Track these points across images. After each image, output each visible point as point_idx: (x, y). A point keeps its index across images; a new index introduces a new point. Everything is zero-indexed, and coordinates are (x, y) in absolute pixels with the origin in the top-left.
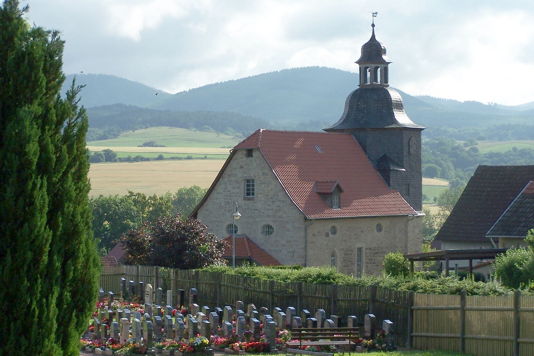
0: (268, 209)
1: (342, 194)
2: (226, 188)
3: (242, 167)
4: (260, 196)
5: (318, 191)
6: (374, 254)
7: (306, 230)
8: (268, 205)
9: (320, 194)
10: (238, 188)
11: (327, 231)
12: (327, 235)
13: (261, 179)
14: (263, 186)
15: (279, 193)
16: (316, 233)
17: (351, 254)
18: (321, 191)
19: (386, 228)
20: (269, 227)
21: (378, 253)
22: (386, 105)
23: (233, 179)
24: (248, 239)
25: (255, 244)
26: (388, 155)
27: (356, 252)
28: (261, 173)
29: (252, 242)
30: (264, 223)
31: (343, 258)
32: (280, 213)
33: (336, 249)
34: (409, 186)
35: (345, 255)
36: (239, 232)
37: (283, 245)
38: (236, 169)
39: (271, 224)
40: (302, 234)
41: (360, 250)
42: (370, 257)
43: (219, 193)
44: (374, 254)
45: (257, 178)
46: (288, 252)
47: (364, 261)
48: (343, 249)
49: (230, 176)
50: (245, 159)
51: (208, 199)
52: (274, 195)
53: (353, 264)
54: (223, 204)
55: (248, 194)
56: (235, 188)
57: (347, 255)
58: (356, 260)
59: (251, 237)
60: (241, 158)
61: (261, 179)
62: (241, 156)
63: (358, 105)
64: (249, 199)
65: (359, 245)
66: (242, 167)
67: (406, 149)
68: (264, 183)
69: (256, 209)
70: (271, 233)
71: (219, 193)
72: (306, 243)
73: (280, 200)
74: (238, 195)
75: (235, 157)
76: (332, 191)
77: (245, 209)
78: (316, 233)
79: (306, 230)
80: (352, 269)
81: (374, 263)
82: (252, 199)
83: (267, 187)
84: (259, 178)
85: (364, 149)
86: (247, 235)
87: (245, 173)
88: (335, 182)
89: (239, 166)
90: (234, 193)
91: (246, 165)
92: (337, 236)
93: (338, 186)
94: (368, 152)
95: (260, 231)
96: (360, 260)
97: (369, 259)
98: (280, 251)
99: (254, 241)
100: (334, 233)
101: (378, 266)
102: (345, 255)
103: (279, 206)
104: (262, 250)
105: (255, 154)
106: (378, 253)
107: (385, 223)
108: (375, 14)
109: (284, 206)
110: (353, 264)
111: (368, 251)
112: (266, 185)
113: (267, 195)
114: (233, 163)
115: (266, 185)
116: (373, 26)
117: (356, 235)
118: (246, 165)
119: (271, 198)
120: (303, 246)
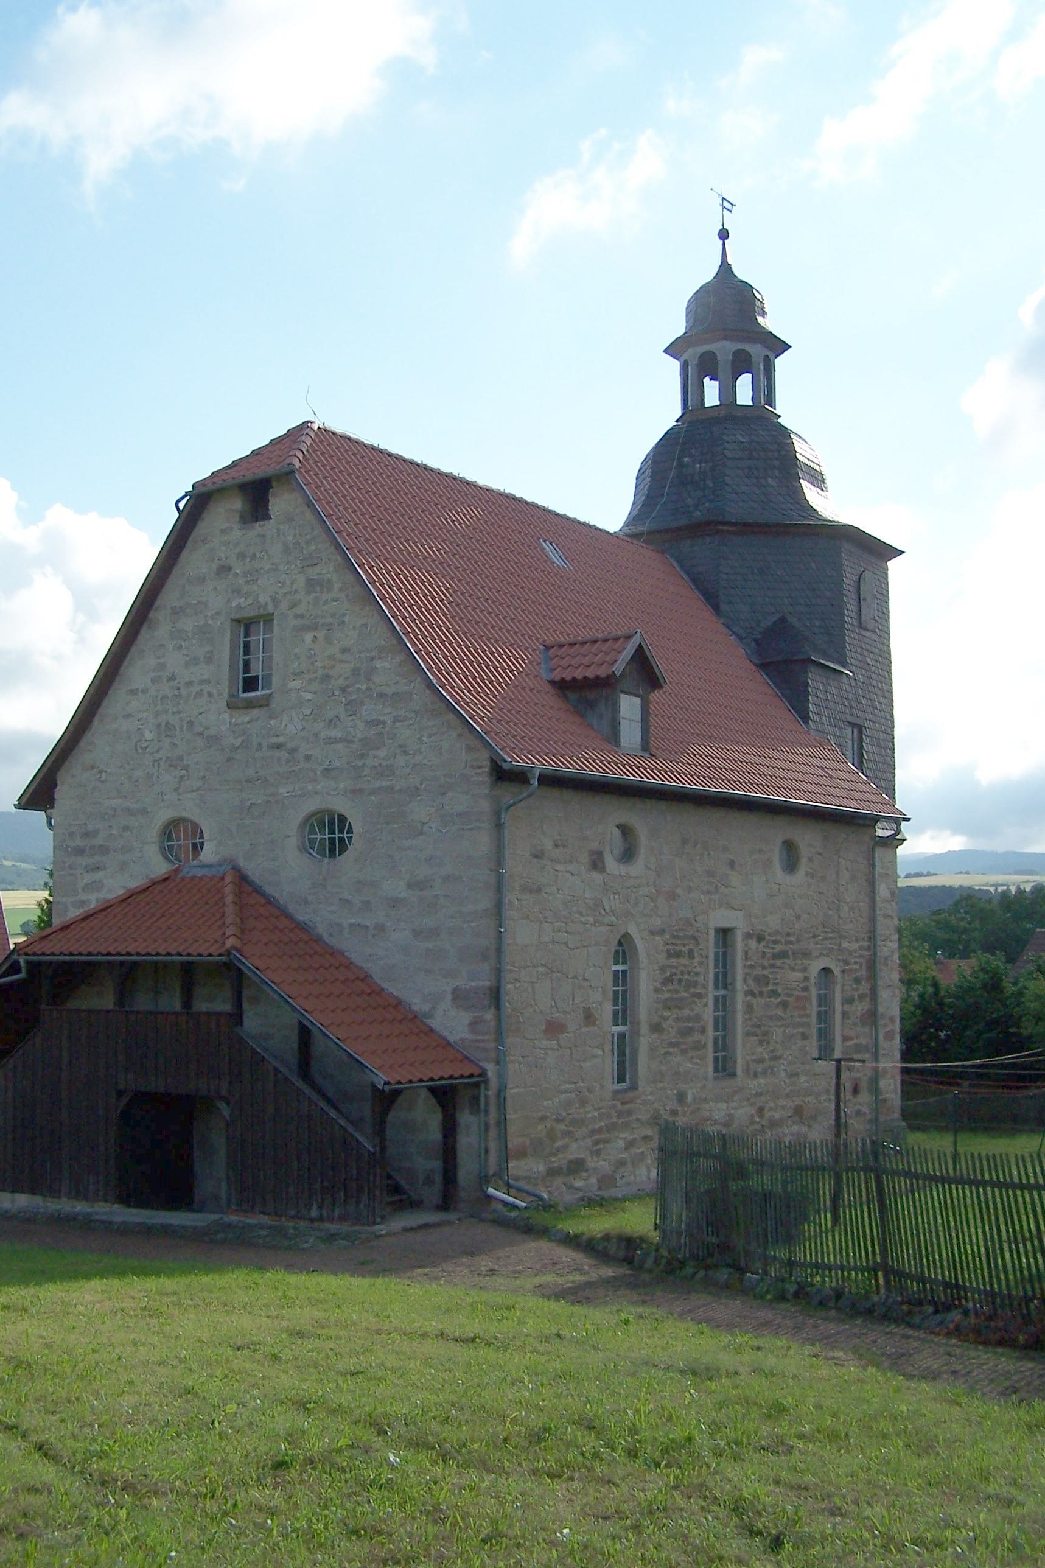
0: (331, 741)
1: (655, 696)
2: (162, 667)
3: (224, 570)
4: (294, 684)
5: (557, 676)
6: (775, 956)
7: (499, 826)
8: (331, 723)
9: (563, 687)
10: (209, 660)
11: (595, 846)
12: (597, 863)
13: (298, 610)
14: (308, 637)
15: (378, 664)
16: (548, 844)
17: (691, 954)
18: (568, 675)
19: (810, 859)
20: (340, 823)
21: (783, 955)
22: (777, 463)
23: (188, 624)
24: (242, 879)
25: (270, 901)
26: (792, 620)
27: (710, 946)
28: (301, 581)
29: (258, 891)
30: (311, 806)
31: (663, 969)
32: (382, 753)
33: (632, 930)
34: (861, 733)
35: (669, 956)
36: (208, 854)
37: (395, 903)
38: (202, 580)
39: (341, 805)
40: (484, 841)
41: (725, 934)
42: (759, 971)
43: (133, 692)
44: (775, 956)
45: (284, 606)
46: (417, 934)
47: (739, 985)
48: (662, 932)
49: (177, 612)
50: (237, 533)
51: (96, 722)
52: (356, 672)
53: (700, 996)
54: (148, 735)
55: (250, 684)
56: (195, 661)
57: (678, 955)
58: (711, 976)
59: (254, 869)
60: (223, 531)
61: (298, 610)
62: (223, 517)
63: (681, 465)
64: (250, 705)
65: (722, 918)
66: (224, 570)
67: (851, 606)
68: (314, 627)
69: (279, 746)
70: (343, 849)
71: (133, 692)
72: (499, 889)
73: (381, 695)
74: (207, 688)
75: (202, 528)
76: (618, 668)
77: (234, 749)
78: (548, 844)
79: (499, 826)
80: (698, 1018)
81: (774, 993)
82: (264, 703)
83: (328, 640)
84: (293, 606)
85: (712, 599)
86: (241, 863)
87: (237, 591)
88: (628, 637)
89: (214, 566)
90: (190, 684)
91: (242, 556)
92: (636, 868)
93: (640, 657)
94: (724, 607)
95: (293, 841)
96: (724, 980)
97: (758, 979)
98: (380, 928)
99: (268, 890)
100: (628, 855)
101: (785, 1005)
102: (669, 956)
103: (377, 723)
104: (302, 927)
105: (280, 503)
106: (783, 955)
107: (808, 838)
108: (727, 205)
109: (396, 719)
110: (700, 996)
111: (753, 944)
112: (321, 634)
113: (326, 678)
114: (193, 561)
115: (321, 634)
116: (724, 235)
117: (710, 873)
118: (242, 556)
119: (343, 690)
120: (485, 903)
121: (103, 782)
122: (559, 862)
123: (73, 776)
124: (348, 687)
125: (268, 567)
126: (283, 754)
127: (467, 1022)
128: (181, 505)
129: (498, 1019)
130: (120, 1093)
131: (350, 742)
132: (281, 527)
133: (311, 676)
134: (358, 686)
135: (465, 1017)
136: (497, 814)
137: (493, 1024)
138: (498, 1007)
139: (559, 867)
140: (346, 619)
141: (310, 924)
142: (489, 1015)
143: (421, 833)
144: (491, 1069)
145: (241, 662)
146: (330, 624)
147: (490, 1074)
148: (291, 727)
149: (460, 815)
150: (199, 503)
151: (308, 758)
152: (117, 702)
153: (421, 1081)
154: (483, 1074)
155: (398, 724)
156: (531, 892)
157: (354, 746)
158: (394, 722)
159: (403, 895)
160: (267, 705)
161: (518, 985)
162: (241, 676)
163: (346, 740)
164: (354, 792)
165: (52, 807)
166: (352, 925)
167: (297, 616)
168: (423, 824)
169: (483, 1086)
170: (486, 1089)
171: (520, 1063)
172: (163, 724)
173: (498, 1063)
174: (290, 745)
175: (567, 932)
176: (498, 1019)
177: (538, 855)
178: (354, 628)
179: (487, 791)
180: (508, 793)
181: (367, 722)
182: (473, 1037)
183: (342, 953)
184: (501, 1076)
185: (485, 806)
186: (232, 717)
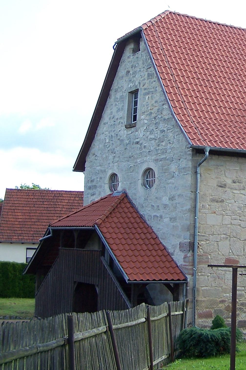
13: (145, 87)
16: (229, 182)
37: (165, 206)
40: (189, 179)
43: (105, 124)
45: (142, 85)
61: (145, 87)
68: (148, 94)
73: (165, 119)
95: (140, 182)
115: (150, 96)
120: (188, 205)
121: (96, 160)
122: (236, 189)
123: (90, 158)
124: (156, 117)
125: (138, 70)
126: (138, 146)
127: (183, 257)
128: (115, 47)
129: (193, 256)
130: (75, 282)
131: (156, 140)
132: (143, 53)
133: (147, 113)
134: (159, 116)
135: (182, 255)
136: (196, 168)
137: (191, 258)
138: (193, 251)
139: (235, 191)
140: (157, 89)
141: (143, 215)
142: (189, 254)
143: (173, 177)
144: (189, 277)
145: (133, 109)
146: (153, 92)
147: (188, 280)
148: (141, 134)
149: (183, 168)
150: (121, 46)
151: (145, 147)
152: (103, 129)
153: (161, 280)
154: (186, 279)
155: (168, 131)
156: (217, 202)
157: (157, 141)
158: (167, 130)
159: (167, 203)
160: (135, 126)
161: (207, 242)
162: (133, 115)
163: (155, 139)
164: (156, 160)
165: (84, 171)
166: (154, 216)
167: (145, 89)
168: (174, 173)
169: (185, 284)
170: (187, 286)
171: (208, 276)
172: (111, 136)
173: (193, 275)
174: (140, 142)
175: (240, 220)
176: (193, 256)
177: (222, 186)
178: (159, 92)
179: (191, 158)
180: (199, 158)
181: (161, 131)
182: (184, 264)
183: (151, 228)
184: (194, 281)
185: (190, 164)
186: (127, 132)
